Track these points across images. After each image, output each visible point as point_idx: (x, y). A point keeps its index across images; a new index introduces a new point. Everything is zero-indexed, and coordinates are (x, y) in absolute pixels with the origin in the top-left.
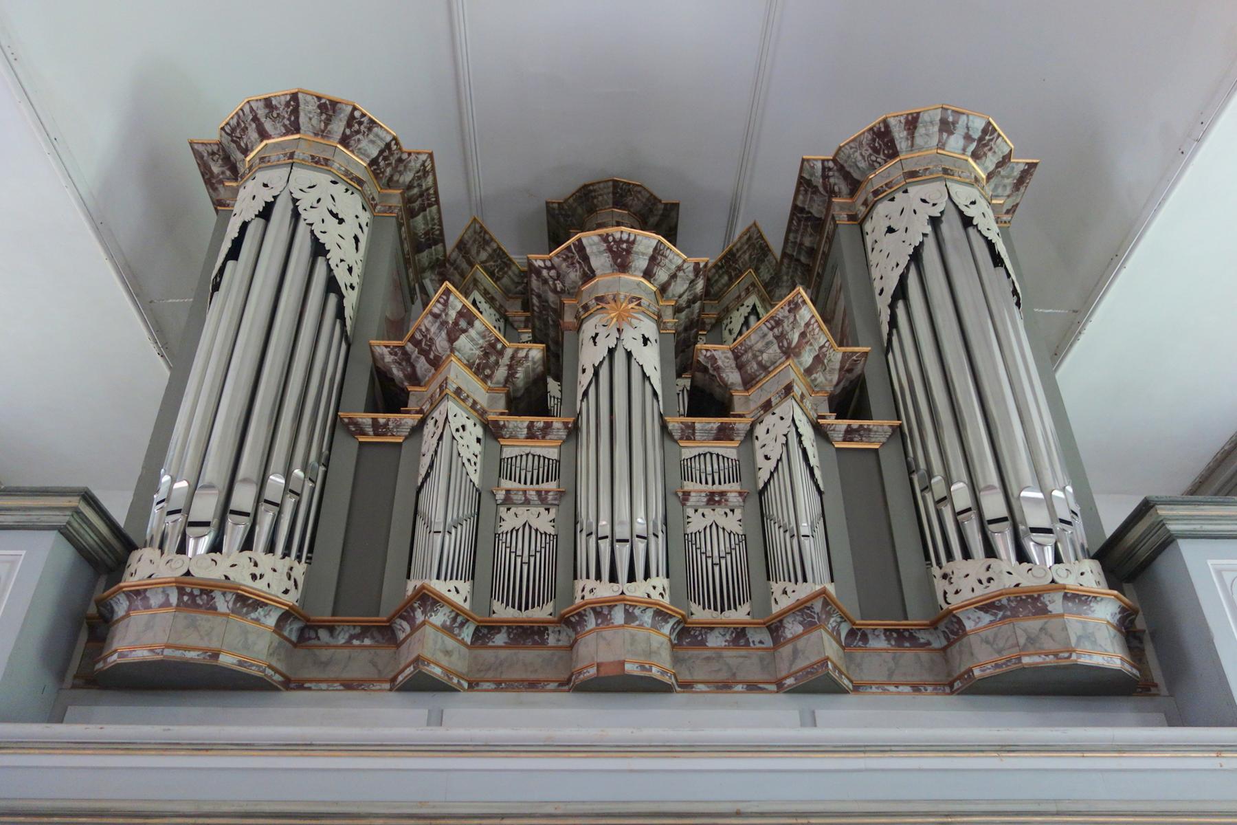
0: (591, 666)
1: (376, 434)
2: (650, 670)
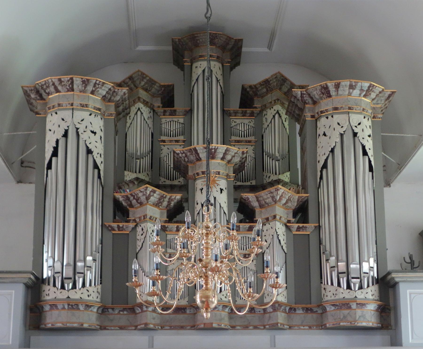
0: (202, 324)
1: (119, 230)
2: (221, 325)
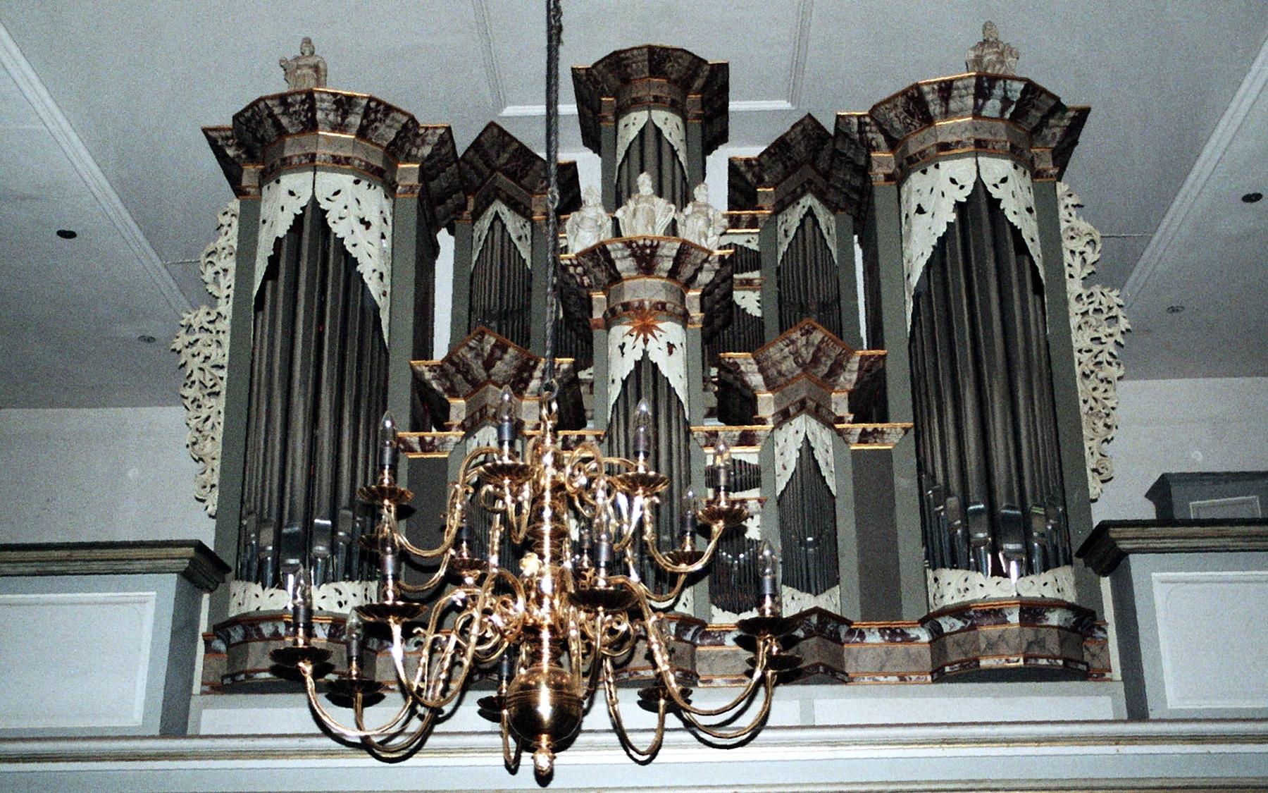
1: (424, 451)
